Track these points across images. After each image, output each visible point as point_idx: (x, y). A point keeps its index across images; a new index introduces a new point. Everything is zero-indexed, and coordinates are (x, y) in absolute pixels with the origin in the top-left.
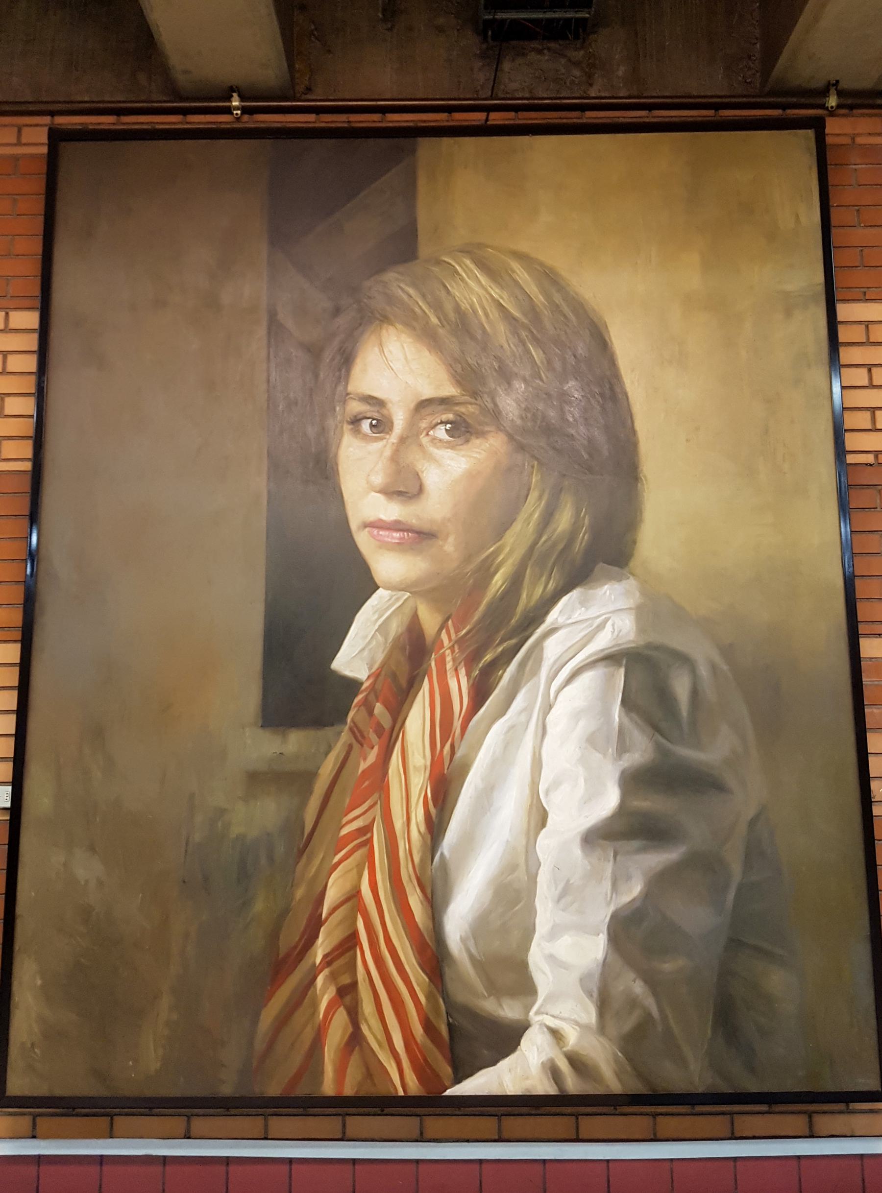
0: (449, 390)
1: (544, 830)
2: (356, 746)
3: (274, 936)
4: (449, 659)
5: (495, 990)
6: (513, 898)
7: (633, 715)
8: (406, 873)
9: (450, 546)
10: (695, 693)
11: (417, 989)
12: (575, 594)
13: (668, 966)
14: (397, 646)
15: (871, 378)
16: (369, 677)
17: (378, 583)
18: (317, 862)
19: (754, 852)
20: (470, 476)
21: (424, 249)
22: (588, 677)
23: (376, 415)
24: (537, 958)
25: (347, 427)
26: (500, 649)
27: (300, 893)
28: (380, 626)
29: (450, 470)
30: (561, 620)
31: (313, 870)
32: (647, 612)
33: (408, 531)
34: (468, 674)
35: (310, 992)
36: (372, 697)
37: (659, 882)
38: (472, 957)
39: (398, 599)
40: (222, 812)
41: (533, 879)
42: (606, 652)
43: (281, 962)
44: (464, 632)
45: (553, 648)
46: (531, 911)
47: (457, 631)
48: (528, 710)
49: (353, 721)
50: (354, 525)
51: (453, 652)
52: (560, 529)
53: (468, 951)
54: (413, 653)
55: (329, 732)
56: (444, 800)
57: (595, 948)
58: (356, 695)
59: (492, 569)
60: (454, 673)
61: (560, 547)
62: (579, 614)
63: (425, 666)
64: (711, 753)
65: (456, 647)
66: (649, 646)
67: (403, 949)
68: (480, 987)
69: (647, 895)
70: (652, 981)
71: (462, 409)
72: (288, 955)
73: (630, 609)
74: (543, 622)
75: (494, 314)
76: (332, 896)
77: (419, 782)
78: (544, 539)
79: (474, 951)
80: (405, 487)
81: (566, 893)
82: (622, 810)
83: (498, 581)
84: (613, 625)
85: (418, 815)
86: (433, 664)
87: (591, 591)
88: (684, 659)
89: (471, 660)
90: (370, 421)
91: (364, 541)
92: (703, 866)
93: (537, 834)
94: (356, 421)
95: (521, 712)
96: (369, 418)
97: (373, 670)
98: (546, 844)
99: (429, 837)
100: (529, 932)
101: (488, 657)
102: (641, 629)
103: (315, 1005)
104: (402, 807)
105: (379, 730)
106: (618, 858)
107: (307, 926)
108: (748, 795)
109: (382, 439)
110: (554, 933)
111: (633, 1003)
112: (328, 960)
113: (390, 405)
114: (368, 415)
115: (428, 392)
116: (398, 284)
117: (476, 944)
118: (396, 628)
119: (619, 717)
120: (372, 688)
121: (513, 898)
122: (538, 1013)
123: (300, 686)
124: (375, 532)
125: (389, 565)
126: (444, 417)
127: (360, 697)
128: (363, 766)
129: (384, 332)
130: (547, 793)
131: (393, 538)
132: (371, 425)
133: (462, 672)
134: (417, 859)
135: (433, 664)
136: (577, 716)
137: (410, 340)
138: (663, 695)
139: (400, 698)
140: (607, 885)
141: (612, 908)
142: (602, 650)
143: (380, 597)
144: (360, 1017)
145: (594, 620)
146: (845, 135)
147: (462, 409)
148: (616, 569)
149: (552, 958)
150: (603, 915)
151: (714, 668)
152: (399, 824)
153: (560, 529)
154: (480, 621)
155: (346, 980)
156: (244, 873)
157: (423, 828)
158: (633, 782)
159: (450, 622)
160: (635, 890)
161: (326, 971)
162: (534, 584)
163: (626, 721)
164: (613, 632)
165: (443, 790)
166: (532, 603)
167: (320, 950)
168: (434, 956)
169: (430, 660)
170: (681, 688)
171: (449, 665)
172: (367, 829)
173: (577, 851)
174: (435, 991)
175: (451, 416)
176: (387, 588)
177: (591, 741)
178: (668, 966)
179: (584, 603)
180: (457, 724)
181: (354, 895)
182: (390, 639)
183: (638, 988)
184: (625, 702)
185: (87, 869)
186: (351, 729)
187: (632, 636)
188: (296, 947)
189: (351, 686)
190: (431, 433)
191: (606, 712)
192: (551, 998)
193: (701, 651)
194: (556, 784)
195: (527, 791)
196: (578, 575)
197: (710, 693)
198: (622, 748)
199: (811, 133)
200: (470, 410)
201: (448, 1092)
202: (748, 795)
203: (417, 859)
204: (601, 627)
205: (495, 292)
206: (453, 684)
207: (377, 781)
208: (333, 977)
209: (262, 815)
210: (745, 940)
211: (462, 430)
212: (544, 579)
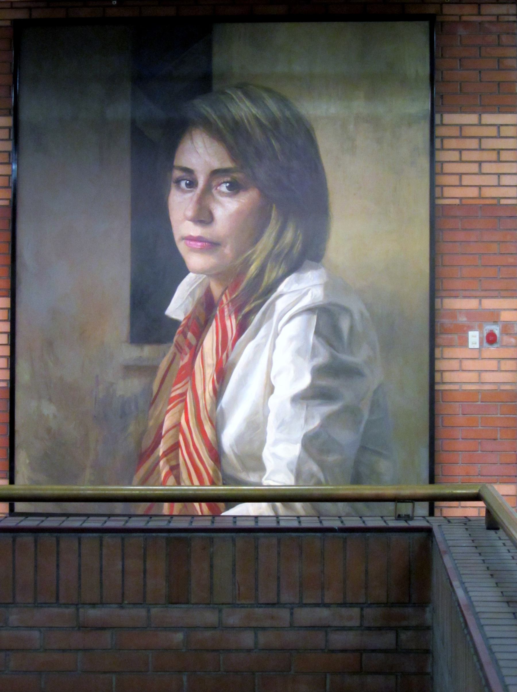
0: (228, 164)
1: (272, 397)
2: (178, 355)
3: (139, 443)
4: (226, 310)
5: (247, 469)
6: (256, 427)
7: (320, 339)
8: (203, 415)
9: (227, 250)
10: (352, 328)
11: (207, 466)
12: (293, 277)
13: (331, 458)
14: (199, 303)
15: (480, 145)
16: (184, 319)
17: (190, 270)
18: (160, 408)
19: (375, 405)
20: (239, 213)
21: (216, 86)
22: (298, 321)
23: (188, 178)
24: (267, 455)
25: (173, 186)
26: (253, 305)
27: (151, 423)
28: (191, 292)
29: (227, 208)
30: (285, 290)
31: (157, 413)
32: (329, 287)
33: (205, 242)
34: (236, 318)
35: (157, 468)
36: (186, 330)
37: (328, 420)
38: (235, 455)
39: (200, 278)
40: (112, 384)
41: (266, 418)
42: (308, 307)
43: (144, 454)
44: (234, 296)
45: (280, 305)
46: (264, 433)
47: (231, 296)
48: (266, 336)
49: (176, 341)
50: (177, 238)
51: (228, 306)
52: (286, 242)
53: (233, 450)
54: (207, 309)
55: (163, 347)
56: (223, 380)
57: (293, 450)
58: (178, 328)
59: (250, 263)
60: (228, 317)
61: (286, 251)
62: (295, 287)
63: (214, 314)
64: (357, 358)
65: (230, 304)
66: (330, 304)
67: (201, 449)
68: (238, 466)
69: (322, 426)
70: (321, 465)
71: (235, 175)
72: (146, 451)
73: (321, 284)
74: (275, 291)
75: (253, 122)
76: (167, 423)
77: (210, 372)
78: (277, 247)
79: (236, 450)
80: (204, 216)
81: (282, 425)
82: (312, 386)
83: (253, 269)
84: (312, 293)
85: (209, 387)
86: (218, 312)
87: (301, 275)
88: (346, 310)
89: (237, 312)
90: (185, 181)
91: (182, 247)
92: (351, 412)
93: (269, 397)
94: (178, 182)
95: (262, 338)
96: (184, 180)
97: (187, 316)
98: (273, 402)
99: (214, 399)
100: (263, 443)
101: (247, 309)
102: (326, 295)
103: (159, 474)
104: (201, 373)
105: (190, 345)
106: (309, 408)
107: (155, 438)
108: (374, 378)
109: (191, 191)
110: (276, 443)
111: (312, 475)
112: (165, 454)
113: (196, 173)
114: (185, 178)
115: (217, 165)
116: (203, 106)
117: (237, 447)
118: (199, 293)
119: (313, 340)
120: (186, 325)
121: (256, 427)
122: (266, 479)
123: (149, 323)
124: (188, 242)
125: (195, 260)
126: (226, 179)
127: (180, 329)
128: (182, 363)
129: (193, 132)
130: (275, 377)
131: (197, 246)
132: (186, 184)
133: (233, 317)
134: (209, 408)
135: (218, 312)
136: (291, 339)
137: (208, 137)
138: (336, 329)
139: (200, 333)
140: (302, 421)
141: (304, 432)
142: (306, 306)
143: (191, 276)
144: (181, 480)
145: (301, 290)
146: (457, 15)
147: (235, 175)
148: (314, 263)
149: (274, 455)
150: (299, 435)
151: (362, 315)
152: (200, 392)
153: (286, 242)
154: (244, 289)
155: (173, 463)
156: (124, 414)
157: (212, 394)
158: (318, 372)
159: (227, 291)
160: (315, 423)
161: (164, 459)
162: (271, 271)
163: (316, 342)
164: (312, 297)
165: (222, 374)
166: (270, 281)
167: (162, 448)
168: (216, 453)
169: (216, 310)
170: (345, 325)
171: (226, 314)
172: (184, 394)
173: (288, 405)
174: (217, 469)
175: (229, 179)
176: (194, 272)
177: (298, 352)
178: (331, 458)
179: (298, 281)
180: (230, 343)
181: (177, 426)
182: (196, 299)
183: (315, 468)
184: (317, 333)
185: (49, 410)
186: (176, 346)
187: (321, 299)
188: (149, 448)
189: (176, 323)
190: (218, 188)
191: (306, 338)
192: (273, 472)
193: (356, 306)
194: (279, 373)
195: (264, 377)
196: (295, 267)
197: (359, 327)
198: (314, 355)
199: (427, 23)
200: (238, 176)
201: (223, 514)
202: (374, 378)
203: (209, 408)
204: (306, 294)
205: (254, 111)
206: (228, 323)
207: (188, 372)
208: (168, 461)
209: (131, 387)
210: (368, 447)
211: (235, 188)
212: (277, 268)
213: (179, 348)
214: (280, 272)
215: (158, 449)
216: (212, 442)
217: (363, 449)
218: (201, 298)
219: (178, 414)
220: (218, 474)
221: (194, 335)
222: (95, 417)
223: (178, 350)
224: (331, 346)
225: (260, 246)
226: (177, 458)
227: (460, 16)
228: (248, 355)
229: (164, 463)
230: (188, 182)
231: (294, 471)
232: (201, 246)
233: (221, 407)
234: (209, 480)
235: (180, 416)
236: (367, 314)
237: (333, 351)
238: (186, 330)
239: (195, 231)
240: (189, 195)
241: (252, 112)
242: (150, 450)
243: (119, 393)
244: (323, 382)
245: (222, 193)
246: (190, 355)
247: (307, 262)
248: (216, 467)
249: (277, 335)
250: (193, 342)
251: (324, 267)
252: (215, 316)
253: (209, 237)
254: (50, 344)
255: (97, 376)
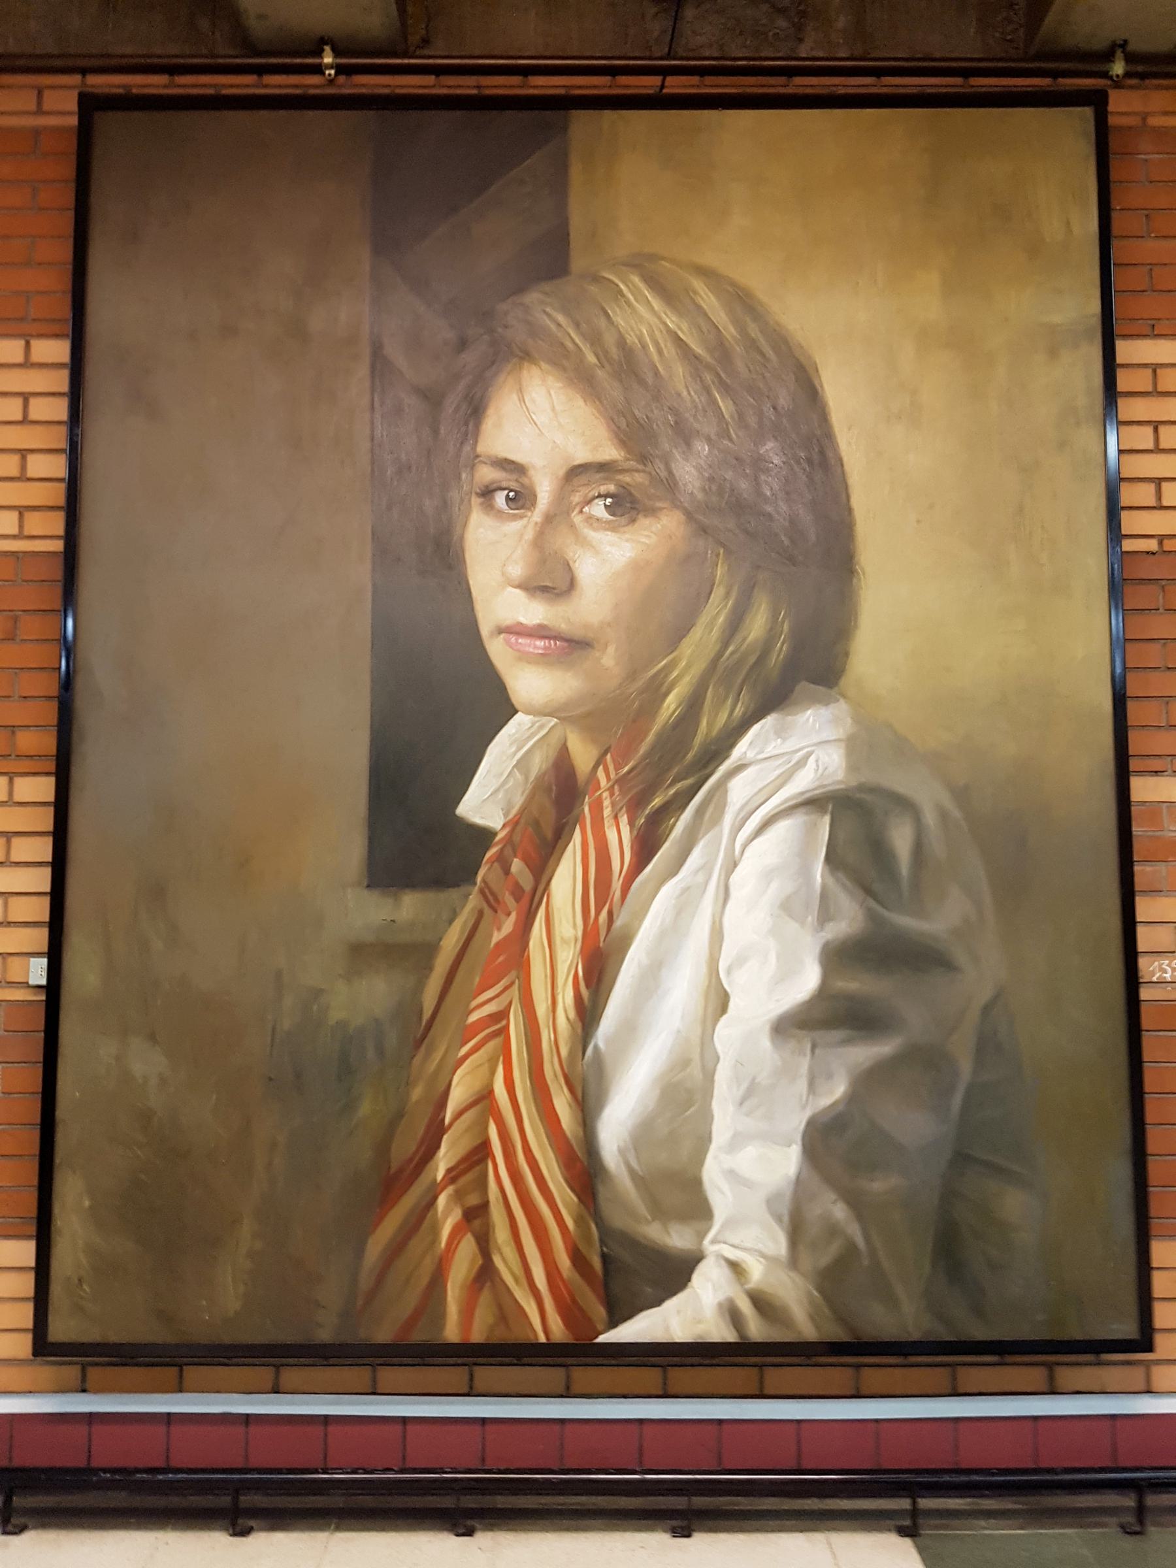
0: (610, 452)
1: (724, 1017)
2: (487, 911)
4: (607, 803)
5: (660, 1212)
7: (840, 875)
8: (551, 1069)
9: (609, 659)
12: (769, 721)
14: (540, 787)
16: (504, 826)
17: (517, 706)
18: (438, 1056)
19: (988, 1045)
20: (636, 567)
21: (578, 262)
22: (783, 827)
23: (513, 485)
24: (712, 1173)
25: (476, 501)
26: (672, 792)
27: (417, 1093)
28: (519, 762)
29: (611, 559)
30: (751, 755)
31: (432, 1066)
32: (859, 747)
33: (555, 638)
34: (631, 823)
36: (508, 851)
37: (868, 1082)
39: (541, 727)
40: (318, 993)
41: (709, 1077)
45: (739, 790)
46: (706, 1116)
49: (484, 881)
50: (485, 630)
51: (612, 795)
54: (561, 795)
55: (453, 894)
56: (599, 980)
58: (487, 849)
59: (664, 689)
60: (612, 821)
61: (752, 660)
62: (774, 747)
63: (576, 812)
64: (937, 921)
66: (861, 788)
68: (642, 1209)
69: (852, 1098)
70: (854, 1201)
71: (626, 478)
72: (401, 1170)
74: (727, 757)
75: (670, 350)
76: (458, 1096)
77: (568, 958)
79: (634, 1164)
80: (551, 580)
81: (750, 1094)
82: (823, 993)
83: (671, 704)
85: (566, 997)
86: (586, 809)
89: (635, 805)
91: (498, 650)
92: (923, 1063)
94: (487, 493)
97: (511, 816)
98: (726, 1034)
100: (703, 1142)
101: (657, 802)
102: (852, 766)
103: (435, 1230)
105: (517, 892)
106: (817, 1051)
108: (982, 974)
110: (736, 1142)
111: (833, 1230)
113: (531, 472)
114: (504, 484)
115: (582, 455)
116: (545, 310)
118: (539, 763)
120: (509, 840)
123: (417, 840)
125: (530, 683)
126: (603, 489)
127: (493, 851)
128: (497, 937)
130: (729, 972)
131: (536, 647)
133: (624, 820)
134: (564, 1052)
135: (586, 809)
138: (879, 850)
139: (544, 852)
140: (802, 1085)
142: (802, 793)
143: (519, 717)
144: (492, 1245)
145: (793, 754)
147: (626, 478)
150: (796, 1122)
151: (944, 815)
155: (473, 1200)
156: (346, 1069)
157: (572, 1014)
158: (837, 958)
159: (609, 756)
160: (836, 1091)
161: (450, 1190)
162: (719, 703)
163: (831, 881)
166: (714, 733)
168: (585, 1171)
169: (582, 804)
170: (901, 840)
171: (607, 812)
172: (503, 1015)
173: (766, 1043)
175: (612, 488)
176: (528, 713)
177: (786, 907)
179: (781, 732)
180: (617, 885)
181: (485, 1097)
182: (532, 778)
183: (840, 1212)
184: (832, 859)
185: (147, 1063)
186: (482, 891)
187: (840, 775)
188: (411, 1160)
189: (483, 836)
190: (586, 509)
192: (729, 1224)
193: (929, 795)
195: (704, 970)
196: (773, 697)
198: (825, 915)
199: (1088, 112)
201: (602, 1339)
202: (982, 974)
203: (564, 1052)
206: (612, 835)
208: (458, 1196)
209: (368, 998)
211: (626, 506)
212: (729, 702)
213: (491, 900)
214: (739, 711)
215: (432, 1163)
216: (573, 1142)
217: (962, 1159)
218: (544, 774)
219: (485, 1069)
220: (589, 1229)
221: (531, 109)
222: (271, 1079)
223: (488, 902)
224: (868, 891)
225: (687, 648)
226: (481, 1184)
227: (1144, 117)
228: (659, 912)
229: (447, 1203)
230: (512, 494)
231: (786, 1219)
232: (545, 648)
233: (596, 1047)
234: (565, 1243)
235: (493, 1072)
236: (956, 813)
237: (872, 903)
238: (508, 851)
239: (533, 612)
240: (517, 525)
241: (665, 324)
242: (412, 1166)
243: (336, 1014)
244: (851, 984)
245: (591, 520)
246: (518, 914)
247: (803, 686)
248: (582, 1207)
249: (732, 865)
250: (527, 881)
251: (844, 696)
252: (580, 819)
253: (563, 626)
254: (156, 893)
255: (279, 975)
